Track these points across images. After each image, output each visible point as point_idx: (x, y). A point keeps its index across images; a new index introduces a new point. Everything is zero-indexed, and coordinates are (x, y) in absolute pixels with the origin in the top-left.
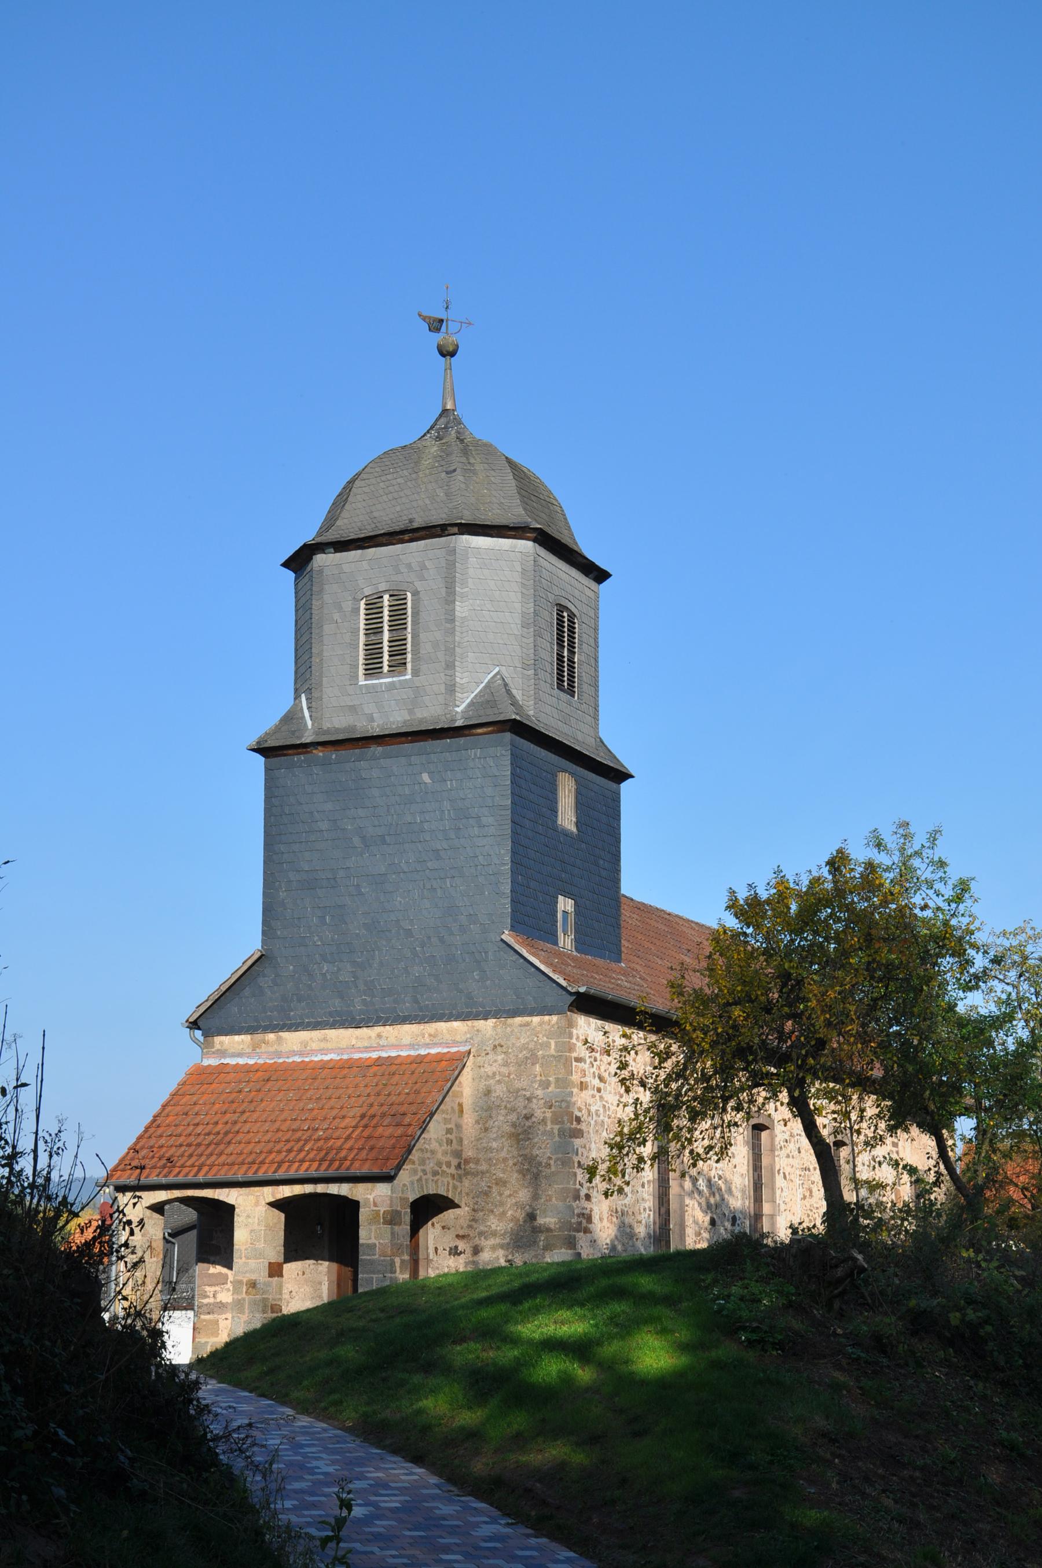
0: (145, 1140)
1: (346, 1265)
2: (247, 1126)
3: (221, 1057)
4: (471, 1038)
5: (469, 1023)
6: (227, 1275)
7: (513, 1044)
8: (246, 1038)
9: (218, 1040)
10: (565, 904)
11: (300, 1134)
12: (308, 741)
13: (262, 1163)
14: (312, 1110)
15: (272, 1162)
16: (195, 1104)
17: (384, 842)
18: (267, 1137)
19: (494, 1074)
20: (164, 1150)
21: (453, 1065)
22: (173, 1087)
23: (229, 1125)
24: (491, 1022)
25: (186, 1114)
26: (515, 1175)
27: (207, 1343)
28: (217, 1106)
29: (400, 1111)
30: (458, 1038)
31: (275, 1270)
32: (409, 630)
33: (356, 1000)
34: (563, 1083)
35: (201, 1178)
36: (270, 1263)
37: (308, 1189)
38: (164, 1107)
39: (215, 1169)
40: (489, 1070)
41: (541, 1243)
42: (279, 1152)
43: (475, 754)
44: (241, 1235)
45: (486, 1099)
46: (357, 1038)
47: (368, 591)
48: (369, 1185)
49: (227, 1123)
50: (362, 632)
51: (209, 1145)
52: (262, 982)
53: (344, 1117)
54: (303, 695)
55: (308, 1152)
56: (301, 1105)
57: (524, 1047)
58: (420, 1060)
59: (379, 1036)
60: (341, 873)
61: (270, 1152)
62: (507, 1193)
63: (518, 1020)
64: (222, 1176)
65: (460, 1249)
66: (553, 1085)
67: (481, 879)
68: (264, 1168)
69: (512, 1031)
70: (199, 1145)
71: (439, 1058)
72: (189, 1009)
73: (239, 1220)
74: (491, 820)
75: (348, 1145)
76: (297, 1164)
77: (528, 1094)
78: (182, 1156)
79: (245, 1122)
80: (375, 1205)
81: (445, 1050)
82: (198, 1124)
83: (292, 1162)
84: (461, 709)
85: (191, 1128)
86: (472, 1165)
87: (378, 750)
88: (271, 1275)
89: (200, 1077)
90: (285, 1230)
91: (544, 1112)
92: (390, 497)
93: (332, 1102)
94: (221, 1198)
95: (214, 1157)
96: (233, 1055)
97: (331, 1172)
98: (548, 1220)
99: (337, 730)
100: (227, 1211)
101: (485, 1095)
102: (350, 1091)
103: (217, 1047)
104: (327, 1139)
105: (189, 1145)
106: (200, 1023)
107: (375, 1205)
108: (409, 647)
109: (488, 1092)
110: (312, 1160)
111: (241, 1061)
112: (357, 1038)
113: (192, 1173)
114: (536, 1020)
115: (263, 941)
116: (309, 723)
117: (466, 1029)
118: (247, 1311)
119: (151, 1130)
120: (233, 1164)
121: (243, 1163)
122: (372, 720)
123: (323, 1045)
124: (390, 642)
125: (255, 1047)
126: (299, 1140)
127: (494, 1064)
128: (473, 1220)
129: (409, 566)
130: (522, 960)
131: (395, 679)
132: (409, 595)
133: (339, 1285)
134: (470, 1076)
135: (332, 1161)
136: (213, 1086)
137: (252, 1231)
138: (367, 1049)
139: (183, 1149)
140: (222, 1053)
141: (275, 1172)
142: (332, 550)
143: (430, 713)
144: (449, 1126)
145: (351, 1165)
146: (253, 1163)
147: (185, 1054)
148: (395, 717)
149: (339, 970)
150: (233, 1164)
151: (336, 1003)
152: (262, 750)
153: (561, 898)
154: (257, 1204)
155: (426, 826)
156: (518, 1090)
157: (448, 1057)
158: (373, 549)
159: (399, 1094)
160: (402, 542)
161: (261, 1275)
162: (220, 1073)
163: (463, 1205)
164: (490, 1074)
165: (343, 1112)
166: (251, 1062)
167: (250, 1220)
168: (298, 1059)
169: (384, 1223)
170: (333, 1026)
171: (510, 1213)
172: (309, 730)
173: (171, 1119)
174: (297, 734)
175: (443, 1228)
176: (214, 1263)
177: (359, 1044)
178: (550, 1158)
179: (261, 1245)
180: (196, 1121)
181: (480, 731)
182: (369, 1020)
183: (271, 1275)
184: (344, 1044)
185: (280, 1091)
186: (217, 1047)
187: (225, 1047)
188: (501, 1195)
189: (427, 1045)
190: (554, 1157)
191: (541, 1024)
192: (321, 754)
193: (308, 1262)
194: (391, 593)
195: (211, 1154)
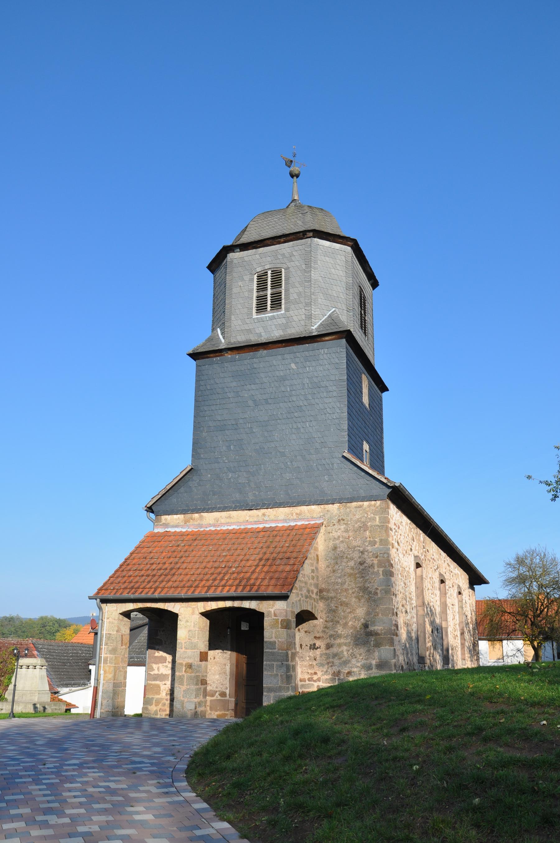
0: (120, 572)
1: (242, 654)
2: (184, 566)
3: (165, 528)
4: (324, 515)
5: (322, 506)
6: (166, 657)
8: (181, 517)
9: (164, 517)
10: (366, 447)
11: (220, 570)
12: (223, 348)
13: (197, 587)
14: (226, 556)
15: (204, 586)
16: (150, 553)
17: (267, 403)
18: (199, 571)
19: (339, 537)
20: (132, 578)
21: (311, 532)
22: (137, 543)
23: (173, 564)
24: (336, 506)
25: (145, 558)
26: (354, 599)
27: (153, 698)
28: (164, 554)
29: (285, 556)
30: (315, 516)
31: (204, 657)
32: (283, 287)
33: (250, 494)
34: (385, 542)
35: (156, 595)
36: (201, 652)
37: (229, 604)
38: (131, 554)
39: (165, 590)
40: (335, 535)
41: (372, 643)
42: (207, 580)
43: (324, 351)
44: (182, 633)
45: (333, 552)
46: (250, 516)
47: (259, 269)
48: (271, 602)
49: (171, 563)
50: (255, 291)
51: (161, 575)
52: (191, 484)
53: (248, 560)
54: (219, 330)
55: (227, 581)
56: (218, 553)
57: (358, 521)
58: (291, 528)
59: (264, 515)
60: (241, 421)
61: (202, 580)
62: (349, 610)
63: (354, 504)
64: (170, 595)
65: (317, 645)
66: (378, 544)
67: (328, 422)
68: (198, 590)
69: (350, 511)
70: (154, 576)
71: (305, 527)
72: (148, 500)
73: (181, 624)
74: (334, 388)
75: (254, 576)
76: (221, 588)
77: (361, 549)
78: (144, 582)
79: (183, 563)
80: (275, 615)
81: (307, 523)
82: (153, 564)
83: (217, 586)
84: (314, 328)
85: (149, 566)
86: (325, 593)
88: (201, 660)
89: (153, 538)
90: (210, 631)
91: (373, 560)
92: (270, 226)
93: (238, 552)
94: (169, 609)
95: (164, 583)
96: (173, 527)
97: (245, 593)
98: (376, 628)
99: (239, 342)
100: (173, 617)
101: (333, 550)
102: (249, 546)
103: (163, 521)
104: (238, 573)
105: (148, 576)
106: (153, 508)
107: (275, 615)
108: (283, 296)
109: (335, 548)
110: (231, 586)
111: (178, 530)
112: (250, 516)
113: (151, 592)
114: (366, 504)
115: (192, 461)
116: (223, 341)
118: (185, 684)
119: (124, 567)
120: (177, 587)
121: (184, 587)
122: (261, 336)
123: (228, 520)
124: (271, 295)
126: (220, 573)
127: (338, 531)
128: (326, 627)
129: (283, 255)
130: (356, 468)
131: (274, 314)
132: (283, 270)
133: (237, 666)
134: (323, 539)
135: (245, 586)
136: (162, 542)
137: (189, 631)
139: (144, 578)
140: (166, 525)
141: (206, 592)
142: (238, 250)
143: (294, 331)
144: (313, 568)
145: (259, 588)
146: (191, 586)
147: (146, 526)
148: (277, 334)
149: (239, 476)
150: (177, 587)
151: (237, 496)
152: (195, 356)
153: (365, 442)
154: (193, 613)
155: (293, 392)
156: (355, 547)
157: (310, 526)
158: (262, 248)
159: (282, 547)
160: (279, 243)
161: (195, 660)
162: (165, 536)
163: (319, 618)
164: (336, 537)
165: (247, 557)
166: (184, 530)
167: (188, 624)
168: (213, 529)
169: (282, 628)
170: (235, 509)
171: (350, 623)
172: (223, 343)
173: (136, 560)
174: (216, 345)
175: (306, 632)
176: (158, 650)
177: (251, 520)
178: (377, 589)
179: (195, 640)
180: (152, 562)
181: (327, 338)
182: (258, 505)
183: (201, 660)
184: (241, 520)
185: (203, 545)
186: (163, 521)
187: (167, 522)
188: (344, 612)
189: (294, 520)
190: (379, 588)
191: (369, 506)
192: (230, 356)
193: (217, 651)
194: (273, 270)
195: (162, 581)
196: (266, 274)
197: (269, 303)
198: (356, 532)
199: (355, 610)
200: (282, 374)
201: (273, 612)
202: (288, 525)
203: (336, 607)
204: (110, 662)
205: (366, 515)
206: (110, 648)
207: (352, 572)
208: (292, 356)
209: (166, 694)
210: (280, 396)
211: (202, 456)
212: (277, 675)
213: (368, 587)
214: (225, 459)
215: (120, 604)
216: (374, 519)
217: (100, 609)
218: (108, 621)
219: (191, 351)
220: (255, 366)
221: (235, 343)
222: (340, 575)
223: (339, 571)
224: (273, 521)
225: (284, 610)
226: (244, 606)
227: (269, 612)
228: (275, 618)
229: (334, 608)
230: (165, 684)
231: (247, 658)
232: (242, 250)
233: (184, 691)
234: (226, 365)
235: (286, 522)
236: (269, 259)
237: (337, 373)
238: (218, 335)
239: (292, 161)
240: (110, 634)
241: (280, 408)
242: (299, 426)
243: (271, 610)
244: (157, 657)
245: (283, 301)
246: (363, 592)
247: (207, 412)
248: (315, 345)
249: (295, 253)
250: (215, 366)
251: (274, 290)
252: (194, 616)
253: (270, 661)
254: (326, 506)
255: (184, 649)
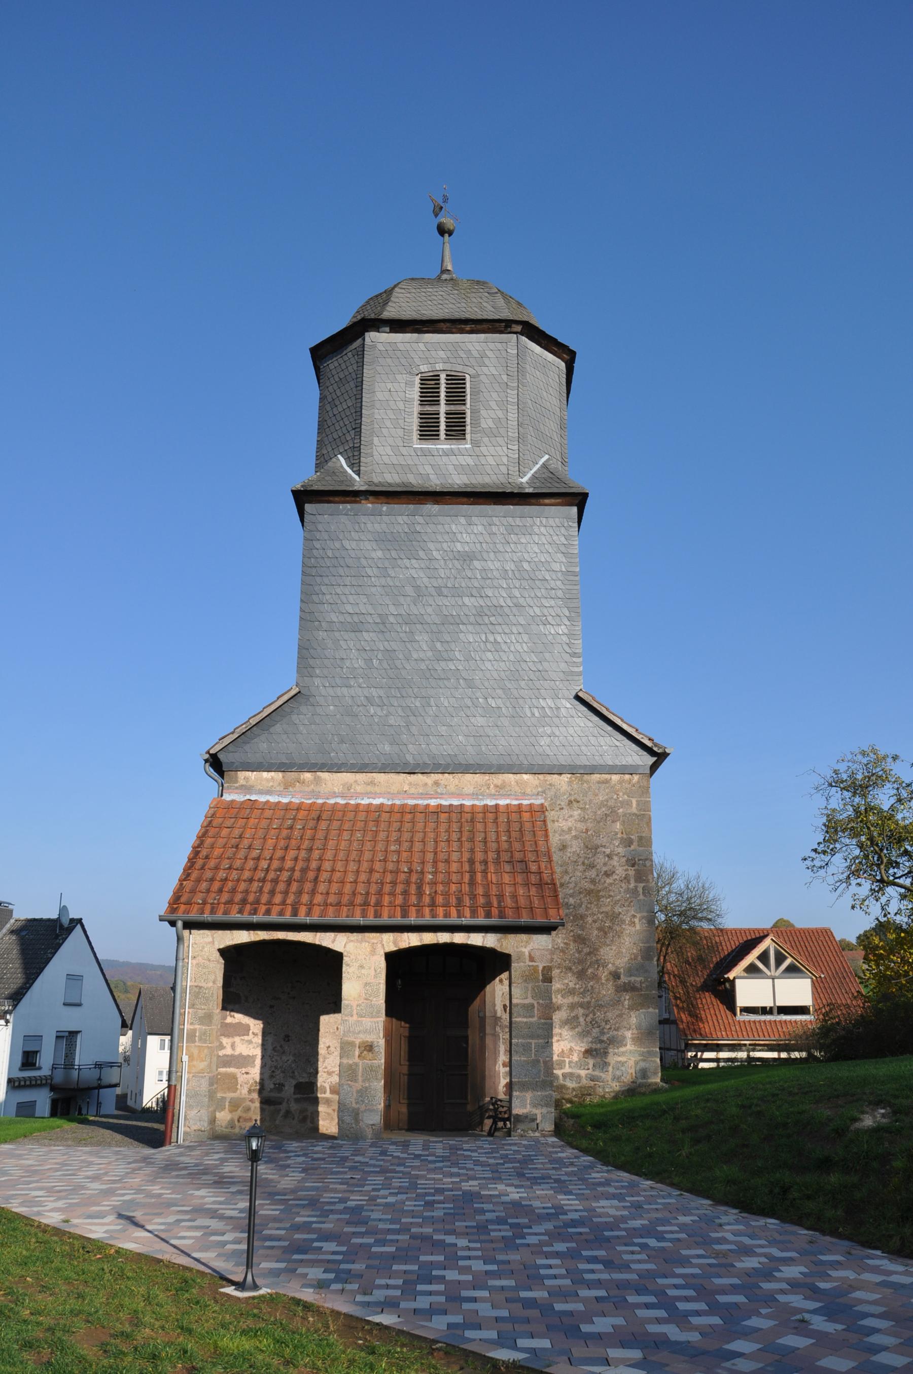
1: (399, 1019)
4: (544, 792)
7: (590, 801)
19: (570, 829)
24: (565, 778)
32: (468, 406)
41: (626, 1002)
44: (350, 989)
46: (410, 784)
47: (424, 368)
48: (524, 937)
57: (602, 804)
59: (436, 783)
69: (590, 787)
72: (210, 742)
73: (348, 972)
77: (608, 851)
80: (532, 959)
84: (525, 481)
87: (433, 508)
96: (261, 792)
99: (390, 485)
100: (334, 960)
103: (242, 782)
107: (532, 959)
108: (468, 420)
111: (273, 799)
112: (410, 784)
114: (615, 778)
117: (537, 782)
118: (360, 1079)
123: (369, 788)
125: (287, 786)
138: (422, 796)
140: (247, 789)
142: (388, 329)
148: (458, 481)
158: (431, 335)
160: (462, 332)
164: (565, 828)
166: (285, 800)
167: (363, 971)
171: (590, 971)
177: (413, 791)
181: (547, 501)
184: (394, 789)
186: (242, 782)
187: (251, 783)
189: (491, 796)
191: (621, 782)
192: (370, 505)
194: (449, 373)
196: (436, 378)
197: (443, 427)
198: (599, 822)
199: (597, 950)
200: (467, 549)
201: (527, 954)
202: (482, 803)
203: (565, 943)
204: (200, 1040)
205: (615, 797)
206: (201, 1013)
207: (592, 887)
208: (484, 521)
209: (250, 1091)
210: (463, 585)
211: (317, 671)
212: (538, 1061)
213: (620, 913)
214: (361, 680)
215: (220, 932)
216: (629, 804)
217: (180, 939)
218: (195, 962)
219: (298, 487)
220: (418, 528)
221: (380, 484)
222: (571, 891)
223: (572, 885)
224: (452, 795)
225: (548, 950)
226: (474, 943)
227: (520, 956)
228: (531, 964)
229: (562, 945)
230: (247, 1073)
231: (410, 1028)
232: (393, 331)
233: (358, 1092)
234: (363, 519)
235: (477, 799)
236: (442, 354)
237: (564, 560)
238: (342, 466)
239: (441, 208)
240: (201, 987)
241: (464, 605)
242: (499, 639)
243: (523, 950)
244: (230, 1024)
245: (468, 428)
246: (611, 920)
247: (328, 597)
248: (527, 509)
249: (489, 353)
250: (343, 519)
251: (452, 408)
252: (375, 957)
253: (523, 1038)
254: (549, 777)
255: (355, 1017)
